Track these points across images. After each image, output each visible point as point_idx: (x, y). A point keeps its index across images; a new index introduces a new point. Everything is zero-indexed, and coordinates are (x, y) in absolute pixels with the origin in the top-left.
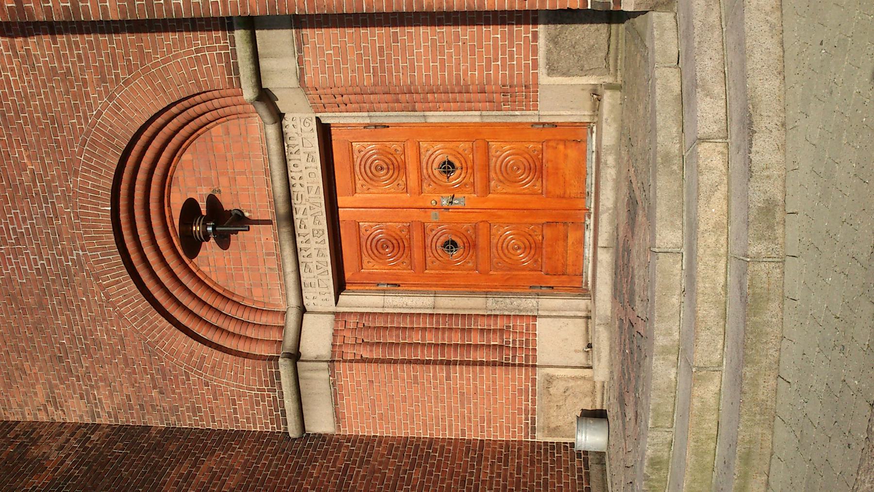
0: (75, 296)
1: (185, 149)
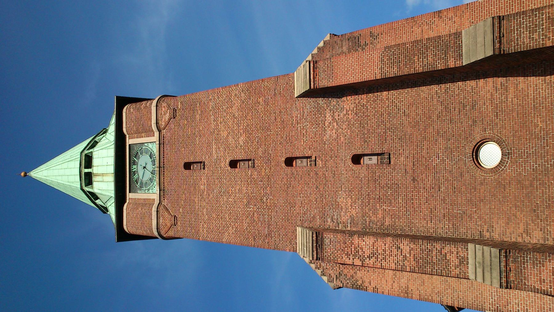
0: (548, 181)
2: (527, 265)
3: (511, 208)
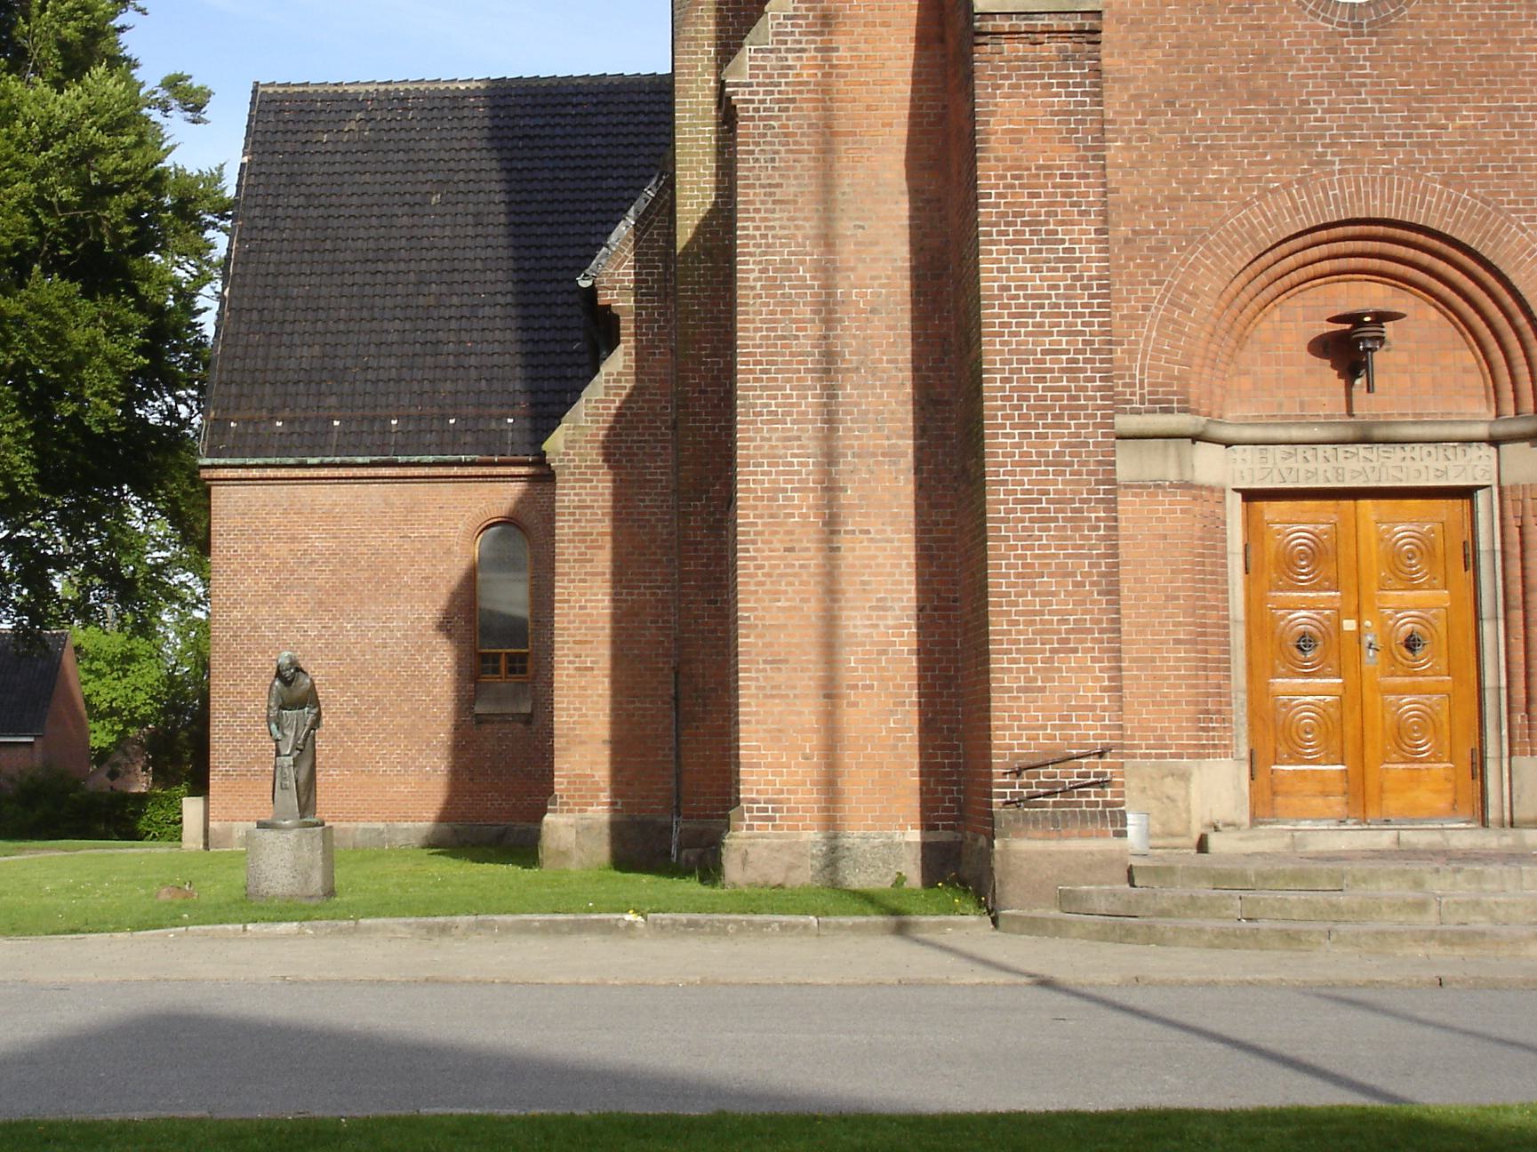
0: (1271, 146)
1: (1444, 314)
2: (1058, 95)
3: (1175, 30)
